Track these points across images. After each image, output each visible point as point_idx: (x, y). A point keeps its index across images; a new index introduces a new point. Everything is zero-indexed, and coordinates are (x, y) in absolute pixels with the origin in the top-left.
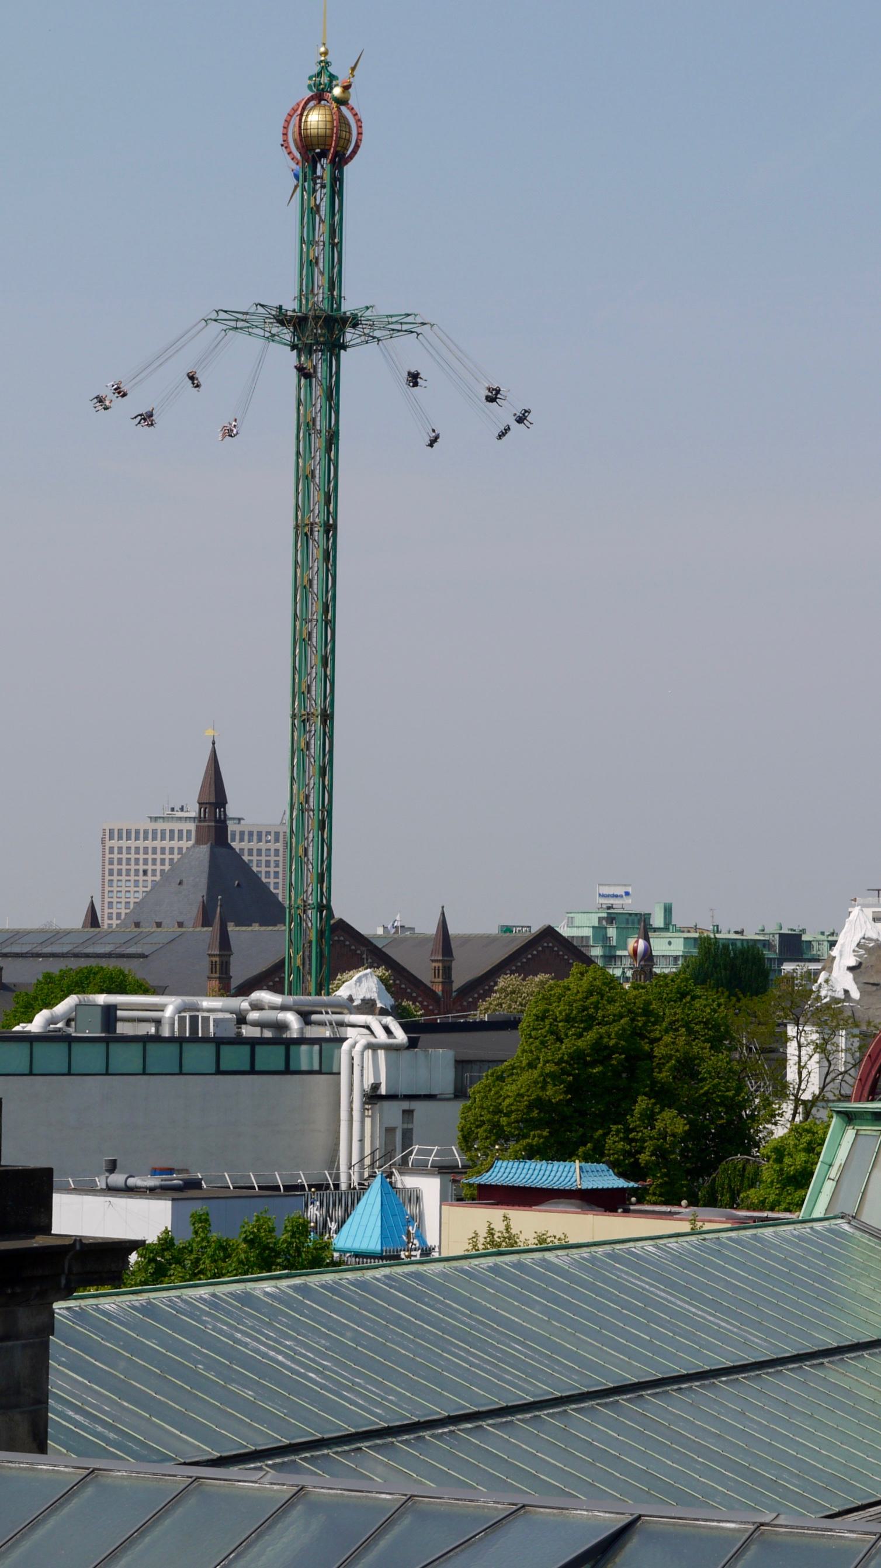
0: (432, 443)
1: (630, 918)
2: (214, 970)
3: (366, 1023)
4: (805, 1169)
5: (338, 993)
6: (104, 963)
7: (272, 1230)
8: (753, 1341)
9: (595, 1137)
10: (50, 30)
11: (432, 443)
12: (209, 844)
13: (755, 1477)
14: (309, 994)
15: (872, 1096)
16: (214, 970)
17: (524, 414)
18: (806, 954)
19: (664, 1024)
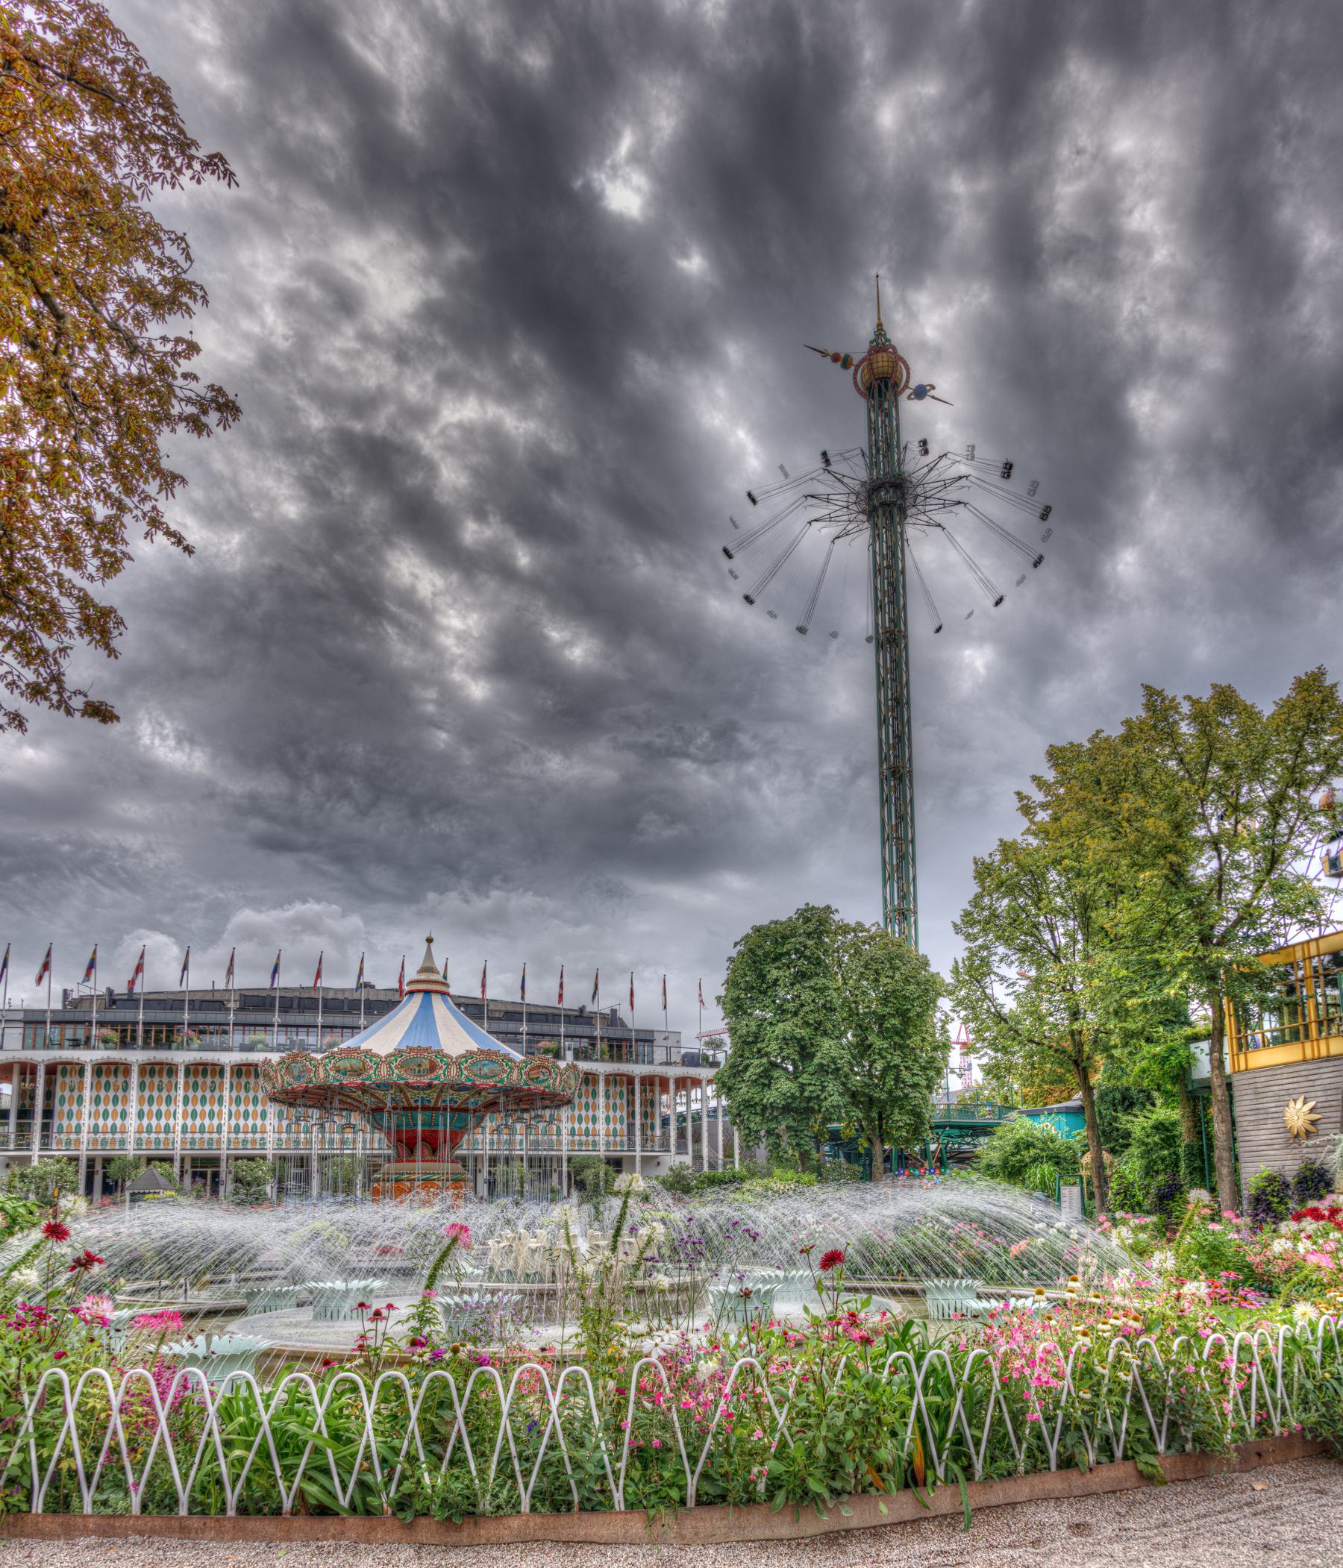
0: (938, 630)
1: (69, 1067)
2: (689, 1125)
3: (869, 640)
4: (891, 525)
5: (474, 1046)
6: (785, 1531)
7: (864, 1558)
8: (634, 1135)
9: (523, 1058)
10: (999, 602)
11: (938, 630)
12: (517, 334)
13: (697, 1139)
14: (85, 1385)
15: (1, 86)
16: (689, 1125)
17: (1169, 1214)
18: (1299, 853)
19: (377, 1244)
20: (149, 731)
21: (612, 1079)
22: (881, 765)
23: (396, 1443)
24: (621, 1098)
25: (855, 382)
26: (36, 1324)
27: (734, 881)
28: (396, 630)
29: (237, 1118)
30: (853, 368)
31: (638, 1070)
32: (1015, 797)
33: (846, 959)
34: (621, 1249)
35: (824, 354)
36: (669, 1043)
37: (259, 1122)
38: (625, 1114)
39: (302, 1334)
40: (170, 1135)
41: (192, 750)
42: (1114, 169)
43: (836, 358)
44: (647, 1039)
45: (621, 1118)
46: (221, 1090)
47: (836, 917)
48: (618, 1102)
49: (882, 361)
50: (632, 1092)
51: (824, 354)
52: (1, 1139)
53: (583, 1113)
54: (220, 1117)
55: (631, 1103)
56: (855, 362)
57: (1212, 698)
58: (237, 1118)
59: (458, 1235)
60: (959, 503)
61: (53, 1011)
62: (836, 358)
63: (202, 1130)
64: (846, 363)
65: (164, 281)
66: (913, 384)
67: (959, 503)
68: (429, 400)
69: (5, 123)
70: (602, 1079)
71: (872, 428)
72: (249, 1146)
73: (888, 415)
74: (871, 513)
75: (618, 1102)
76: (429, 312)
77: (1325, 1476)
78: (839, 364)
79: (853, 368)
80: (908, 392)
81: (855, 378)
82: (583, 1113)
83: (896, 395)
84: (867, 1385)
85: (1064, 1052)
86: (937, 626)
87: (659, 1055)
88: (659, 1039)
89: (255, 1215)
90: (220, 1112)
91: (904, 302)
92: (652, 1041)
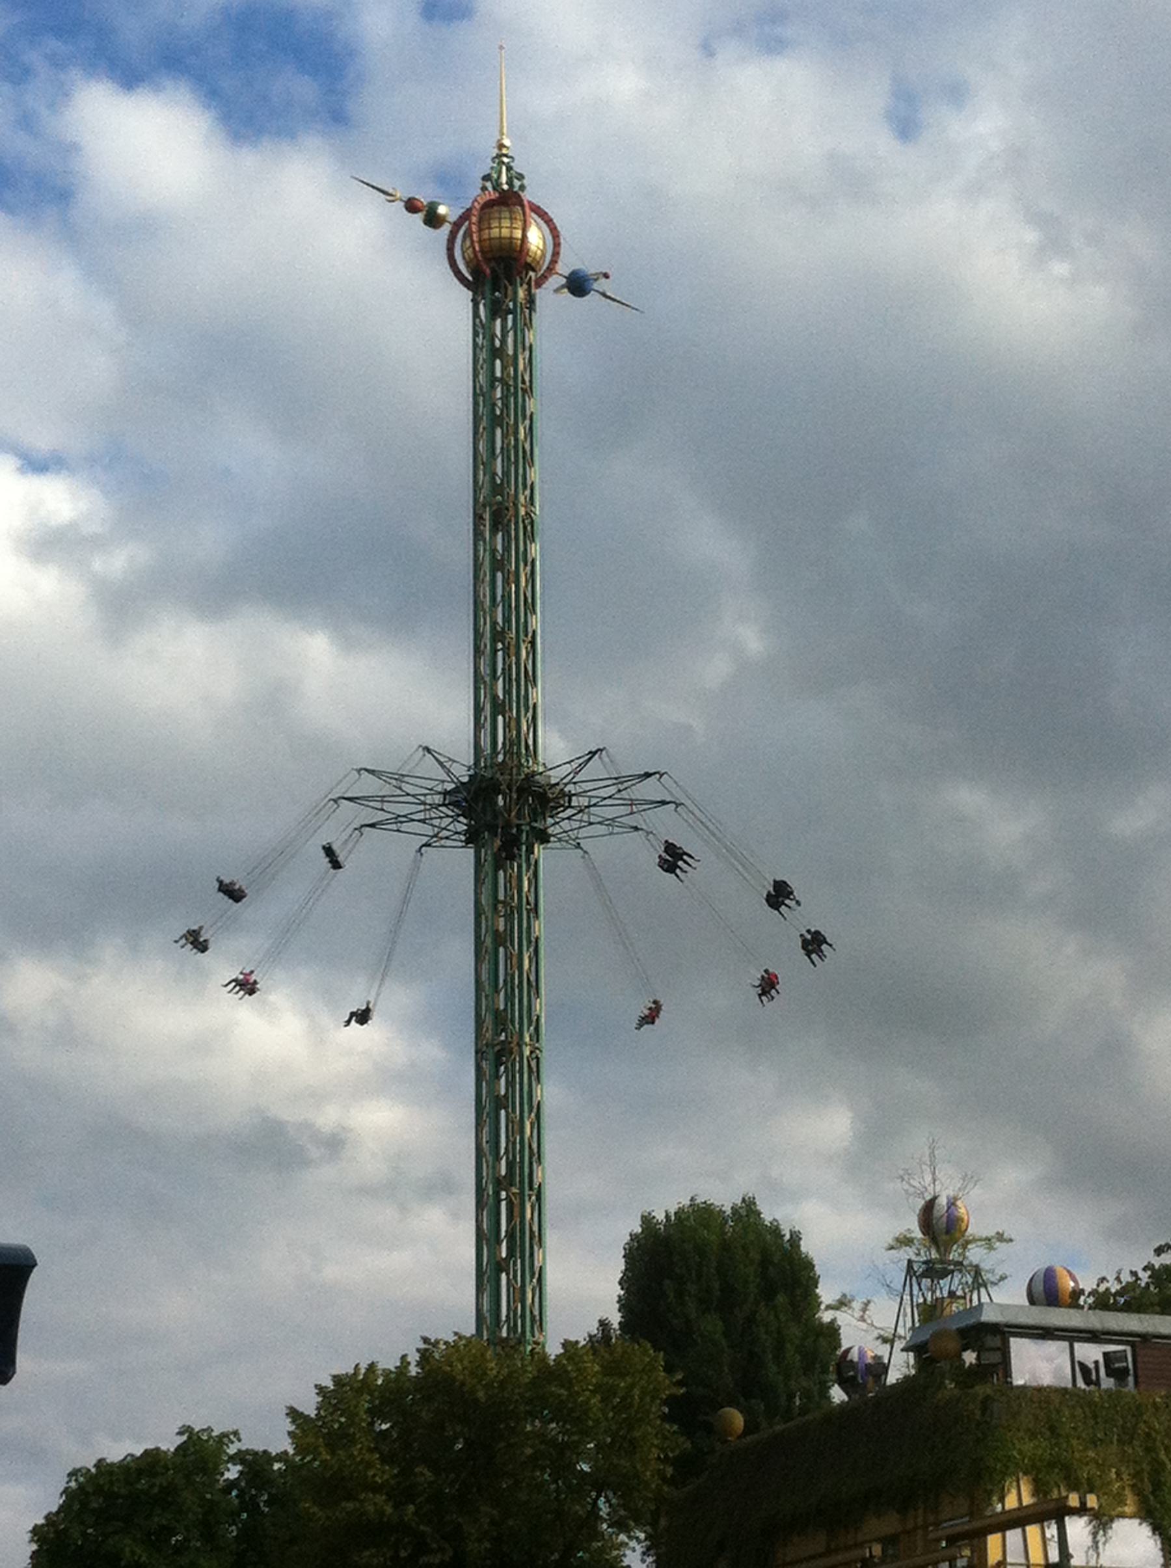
0: (651, 1017)
11: (651, 1017)
20: (585, 1469)
28: (449, 789)
32: (242, 1436)
33: (980, 532)
41: (511, 212)
42: (367, 1425)
47: (292, 1428)
57: (829, 1388)
60: (648, 775)
64: (433, 220)
67: (648, 775)
77: (318, 8)
80: (555, 281)
84: (71, 913)
85: (878, 1268)
86: (241, 883)
89: (43, 477)
91: (543, 255)
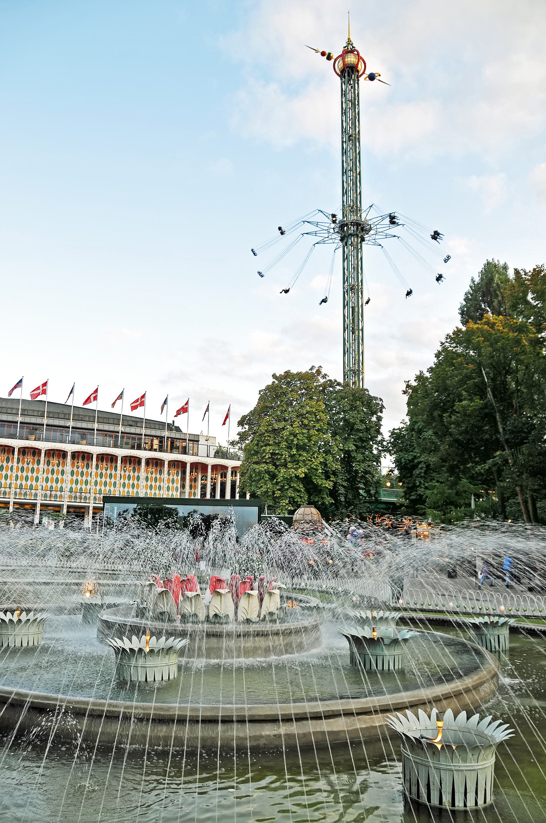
1: (6, 449)
21: (173, 464)
22: (344, 283)
23: (166, 769)
24: (177, 476)
25: (336, 72)
26: (457, 467)
27: (508, 635)
29: (48, 473)
30: (333, 60)
31: (188, 459)
34: (11, 564)
35: (317, 51)
36: (209, 443)
37: (34, 483)
38: (179, 486)
39: (288, 649)
40: (63, 493)
43: (323, 54)
44: (195, 440)
45: (177, 487)
46: (13, 462)
48: (175, 477)
49: (351, 59)
50: (184, 473)
51: (317, 51)
52: (460, 819)
53: (153, 483)
54: (115, 478)
55: (183, 479)
56: (335, 57)
58: (48, 473)
59: (134, 408)
60: (395, 236)
61: (23, 401)
62: (323, 54)
63: (27, 478)
64: (329, 58)
65: (497, 284)
66: (368, 72)
68: (508, 627)
69: (544, 491)
70: (69, 455)
71: (344, 94)
72: (83, 501)
73: (353, 87)
74: (449, 626)
75: (175, 477)
76: (403, 814)
78: (325, 57)
79: (333, 60)
80: (364, 76)
81: (365, 66)
82: (153, 483)
83: (358, 77)
87: (202, 449)
88: (202, 441)
90: (116, 475)
92: (198, 441)
